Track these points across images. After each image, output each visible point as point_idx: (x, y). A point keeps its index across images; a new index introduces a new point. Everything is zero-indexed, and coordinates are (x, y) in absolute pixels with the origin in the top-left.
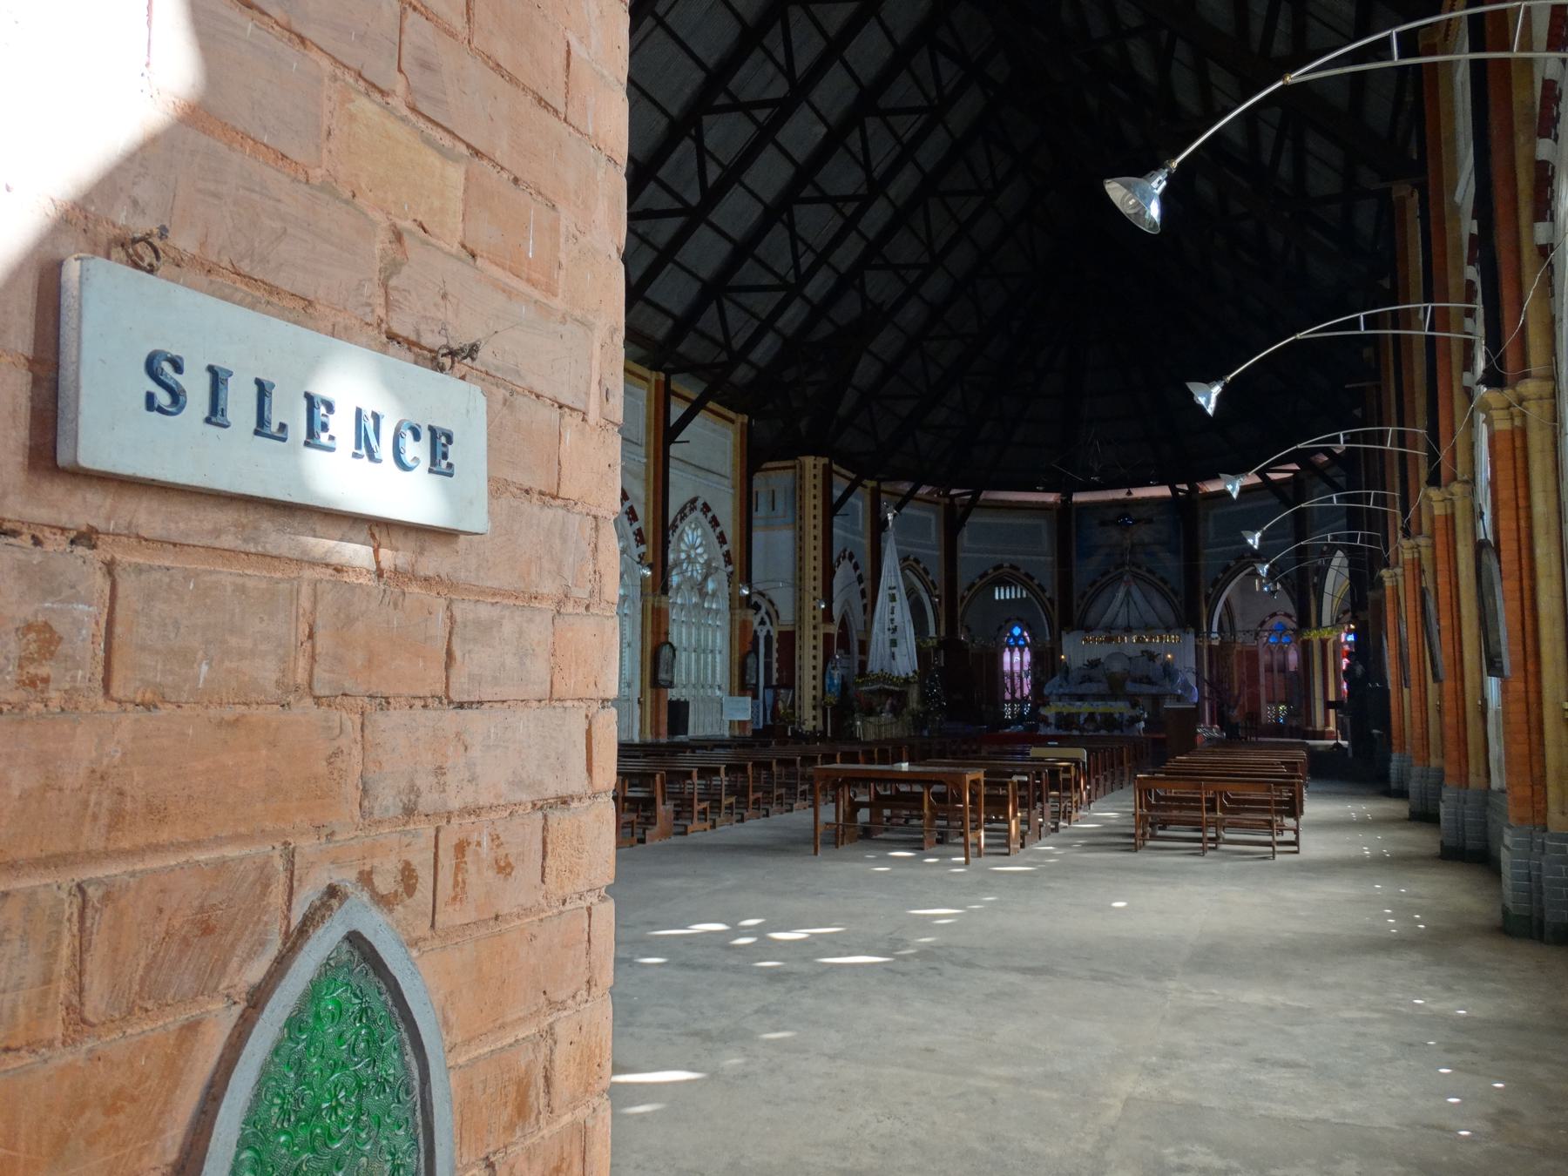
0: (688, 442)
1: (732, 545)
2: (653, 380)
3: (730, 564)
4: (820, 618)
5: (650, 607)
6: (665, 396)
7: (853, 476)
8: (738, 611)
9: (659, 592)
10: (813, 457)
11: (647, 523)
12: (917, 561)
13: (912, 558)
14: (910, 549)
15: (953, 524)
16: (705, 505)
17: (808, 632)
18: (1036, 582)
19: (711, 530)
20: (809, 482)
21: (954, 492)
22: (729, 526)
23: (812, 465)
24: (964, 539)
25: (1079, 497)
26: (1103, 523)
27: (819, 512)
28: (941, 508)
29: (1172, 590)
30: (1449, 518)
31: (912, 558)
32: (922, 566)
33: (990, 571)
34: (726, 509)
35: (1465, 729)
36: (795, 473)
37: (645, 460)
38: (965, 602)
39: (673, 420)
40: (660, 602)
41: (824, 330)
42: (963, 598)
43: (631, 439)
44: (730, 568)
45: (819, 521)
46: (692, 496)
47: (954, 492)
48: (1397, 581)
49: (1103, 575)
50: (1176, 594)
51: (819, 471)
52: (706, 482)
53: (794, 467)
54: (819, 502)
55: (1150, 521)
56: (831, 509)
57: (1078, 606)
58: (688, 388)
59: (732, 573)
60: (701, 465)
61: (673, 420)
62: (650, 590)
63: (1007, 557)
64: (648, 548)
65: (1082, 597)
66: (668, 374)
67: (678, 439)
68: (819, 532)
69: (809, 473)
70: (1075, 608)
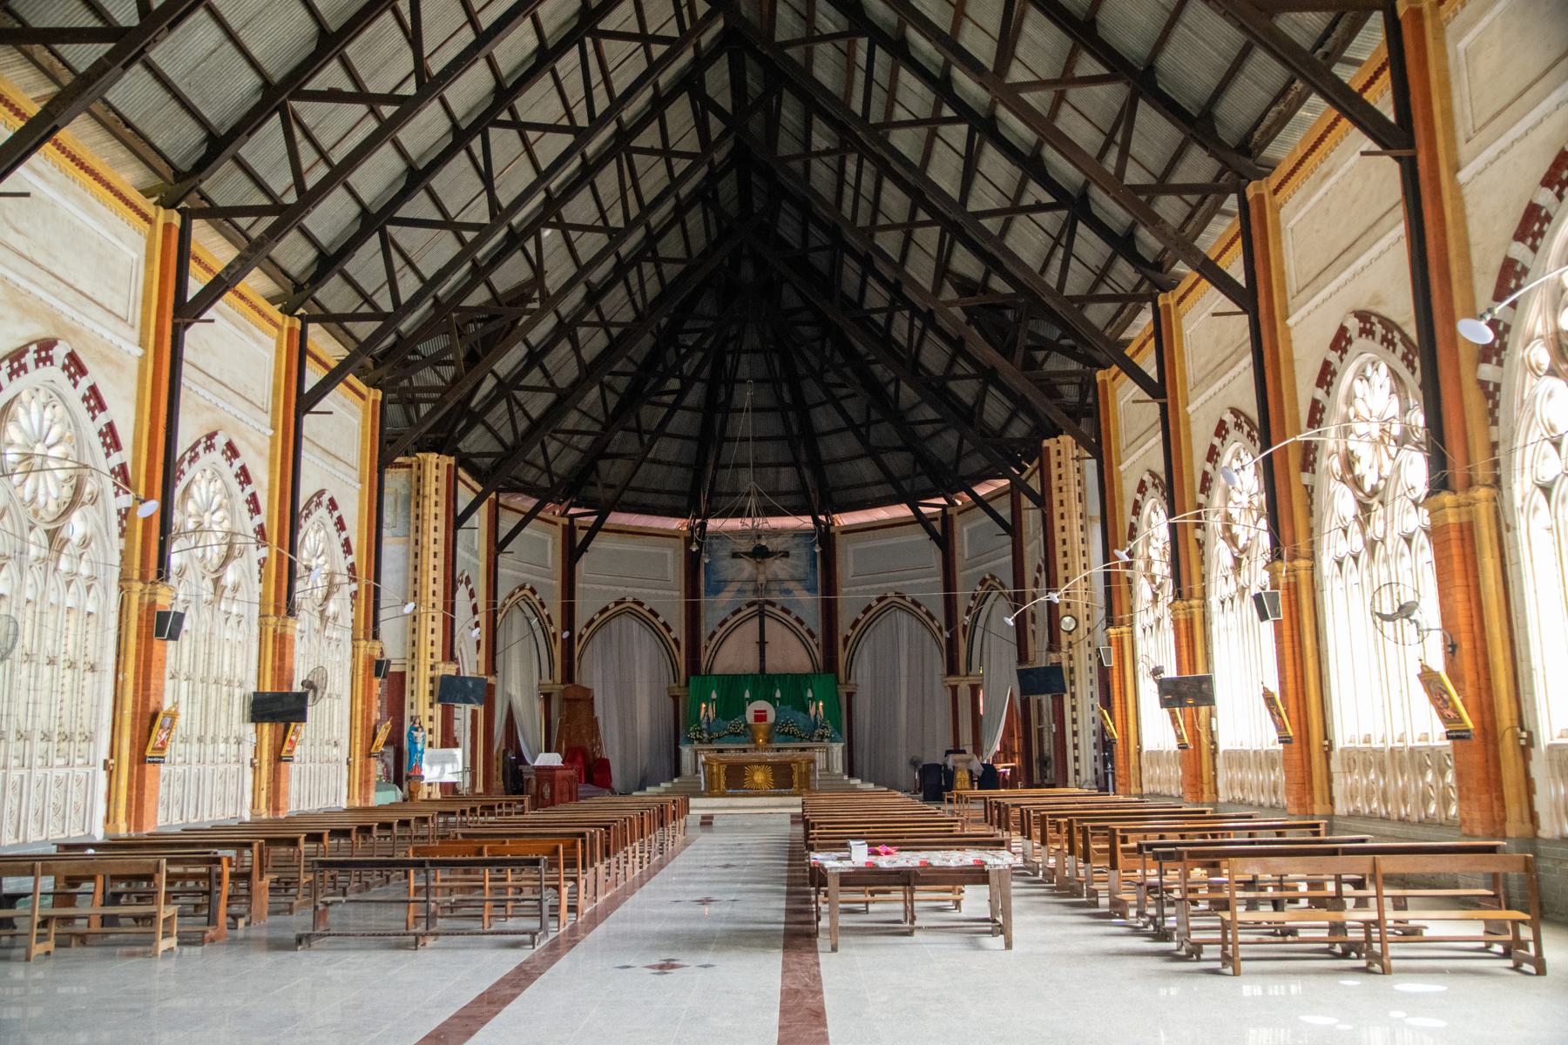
0: (331, 413)
1: (359, 557)
2: (286, 326)
3: (355, 580)
4: (439, 657)
5: (270, 630)
6: (301, 352)
7: (479, 488)
8: (363, 643)
9: (284, 612)
10: (436, 455)
11: (270, 518)
12: (533, 591)
13: (528, 586)
14: (525, 576)
15: (572, 552)
16: (332, 501)
17: (424, 674)
18: (661, 619)
19: (336, 534)
20: (431, 487)
21: (572, 511)
22: (356, 531)
23: (435, 465)
24: (582, 566)
25: (713, 524)
26: (735, 555)
27: (441, 524)
28: (558, 531)
29: (809, 631)
30: (1465, 529)
31: (528, 586)
32: (537, 597)
33: (611, 606)
34: (353, 507)
35: (1498, 767)
36: (411, 473)
37: (270, 432)
38: (583, 640)
39: (308, 386)
40: (284, 626)
41: (479, 296)
42: (581, 636)
43: (255, 400)
44: (354, 587)
45: (441, 535)
46: (318, 489)
47: (572, 511)
48: (1192, 613)
49: (734, 614)
50: (812, 635)
51: (443, 473)
52: (330, 469)
53: (410, 466)
54: (441, 510)
55: (786, 554)
56: (456, 521)
57: (706, 648)
58: (326, 346)
59: (356, 592)
60: (328, 449)
61: (308, 386)
62: (271, 610)
63: (630, 590)
64: (271, 551)
65: (711, 638)
66: (306, 320)
67: (314, 409)
68: (440, 548)
69: (431, 473)
70: (703, 650)
